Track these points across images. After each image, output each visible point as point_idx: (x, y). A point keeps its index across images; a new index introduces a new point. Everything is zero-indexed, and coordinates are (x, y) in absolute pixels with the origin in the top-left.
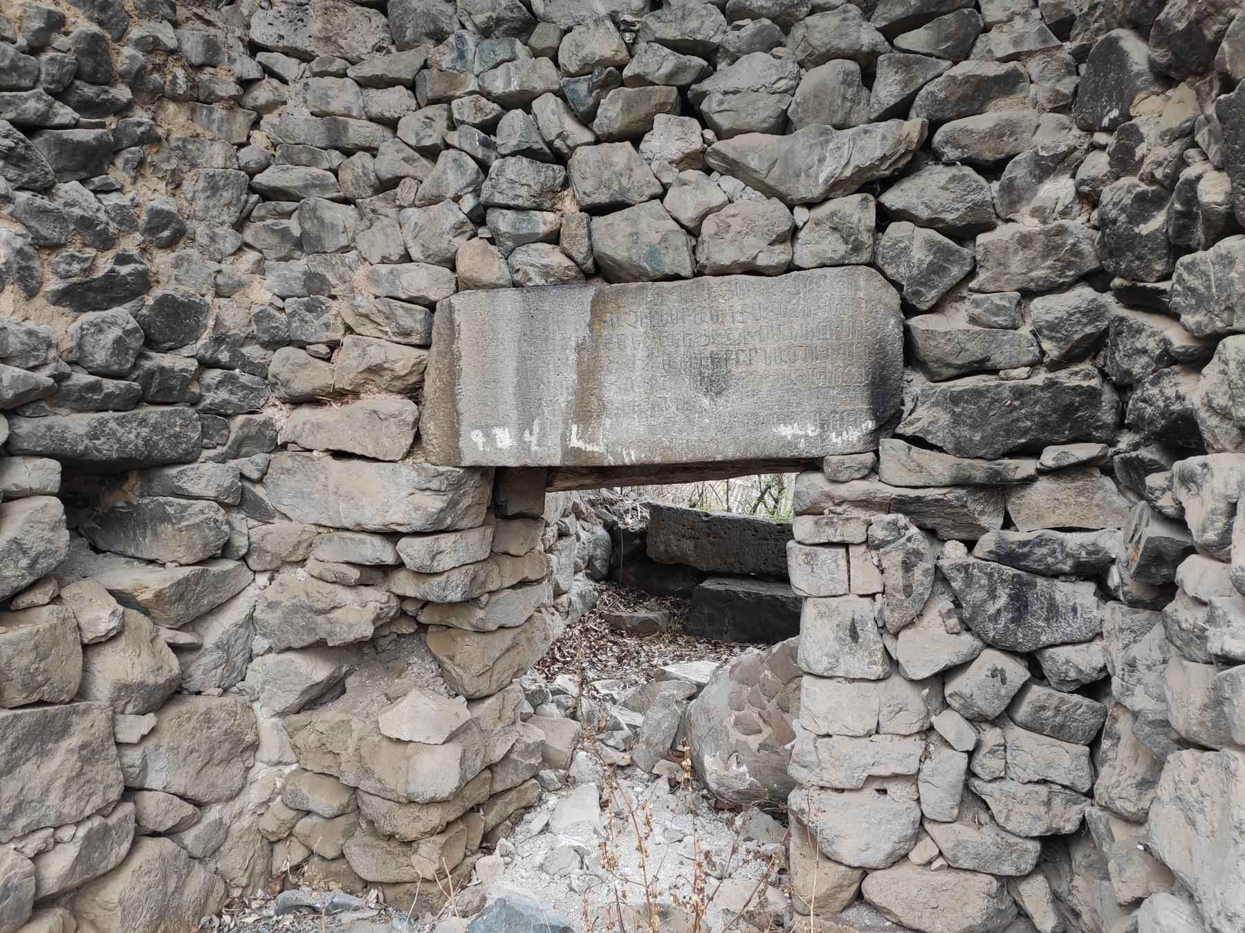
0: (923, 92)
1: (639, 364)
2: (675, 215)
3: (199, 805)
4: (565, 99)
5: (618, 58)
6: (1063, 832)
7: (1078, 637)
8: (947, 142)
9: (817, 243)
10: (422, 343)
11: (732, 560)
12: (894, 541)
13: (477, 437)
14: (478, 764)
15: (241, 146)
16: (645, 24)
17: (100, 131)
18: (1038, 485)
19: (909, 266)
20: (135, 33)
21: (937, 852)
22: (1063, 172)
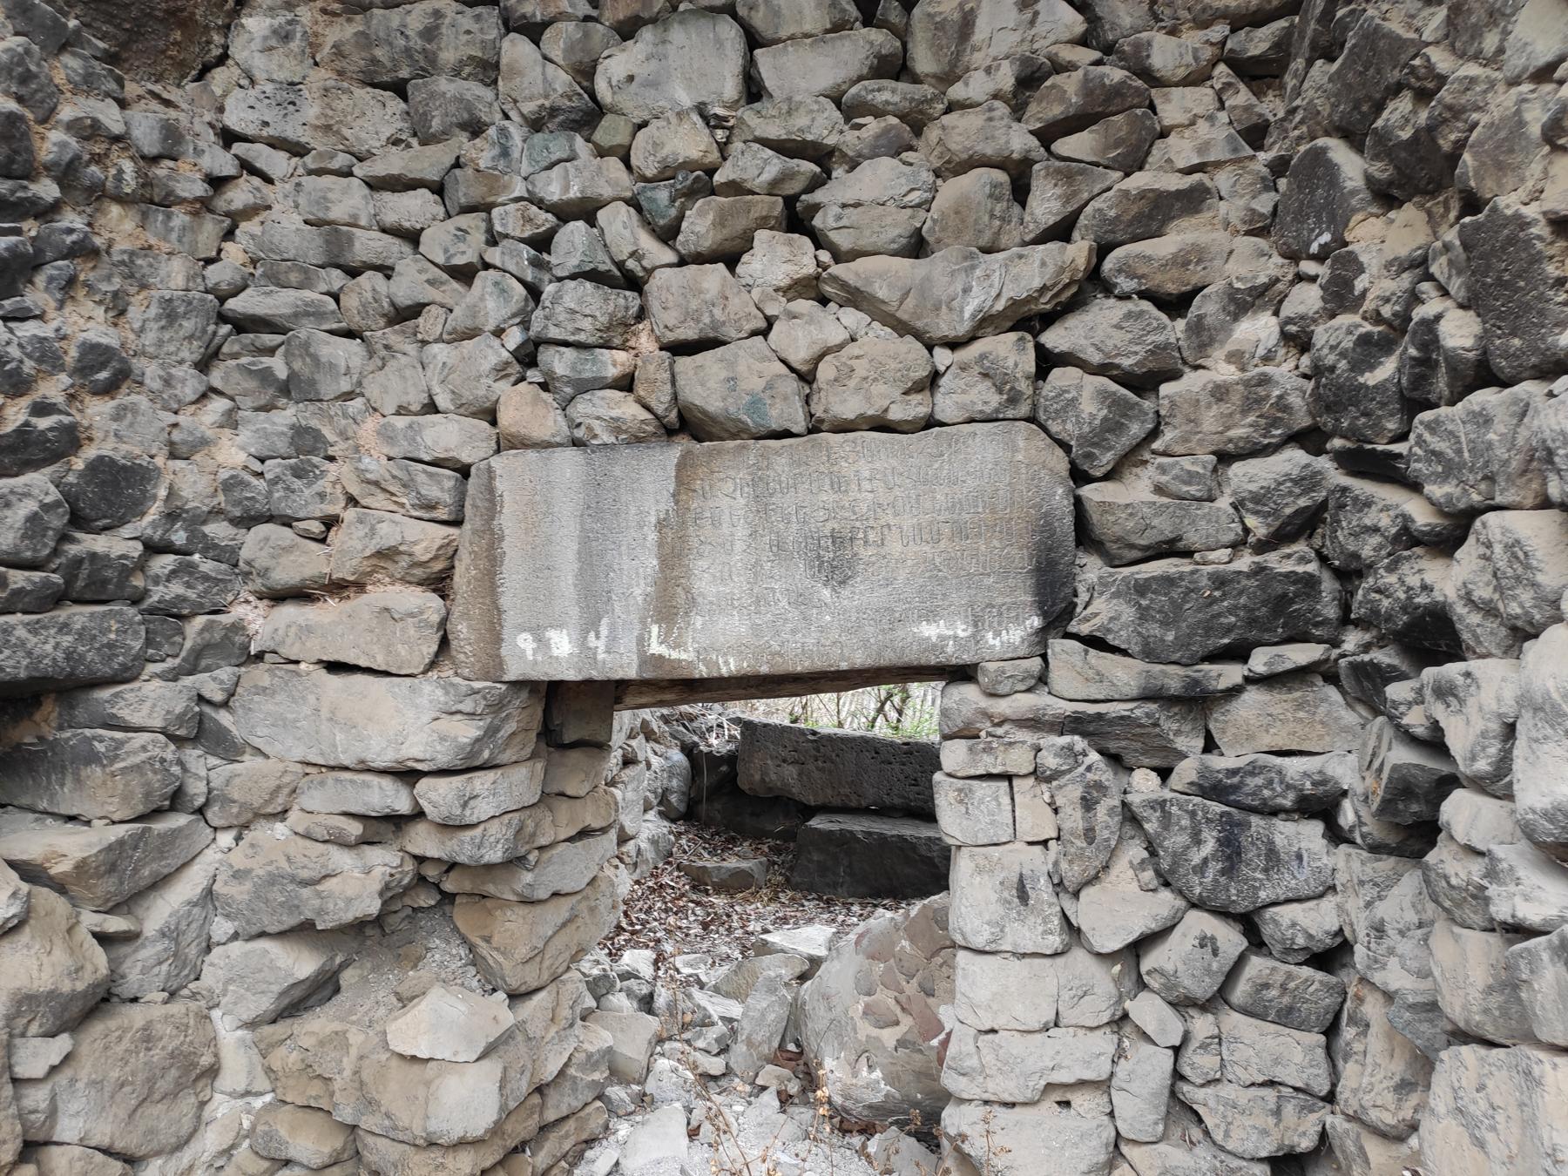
0: (1088, 209)
1: (739, 546)
2: (783, 355)
4: (639, 209)
5: (707, 161)
6: (1298, 1150)
7: (1306, 892)
8: (1120, 271)
9: (964, 392)
10: (452, 518)
12: (1070, 771)
13: (526, 642)
14: (523, 1086)
15: (209, 261)
16: (741, 120)
17: (13, 239)
19: (1078, 422)
20: (66, 113)
22: (1263, 308)
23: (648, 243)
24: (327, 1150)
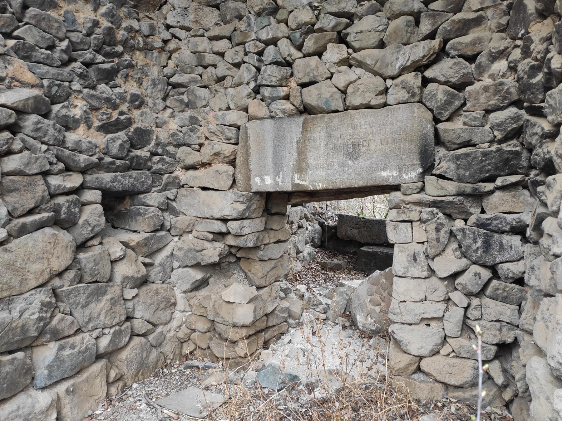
0: (441, 27)
1: (322, 148)
2: (336, 85)
3: (155, 325)
4: (291, 40)
5: (312, 22)
6: (507, 342)
7: (513, 259)
8: (451, 48)
9: (396, 94)
11: (375, 238)
12: (432, 219)
13: (258, 180)
14: (261, 313)
15: (164, 67)
16: (323, 7)
17: (112, 64)
18: (495, 194)
19: (436, 102)
20: (124, 25)
21: (452, 350)
22: (503, 58)
23: (293, 51)
24: (206, 327)
